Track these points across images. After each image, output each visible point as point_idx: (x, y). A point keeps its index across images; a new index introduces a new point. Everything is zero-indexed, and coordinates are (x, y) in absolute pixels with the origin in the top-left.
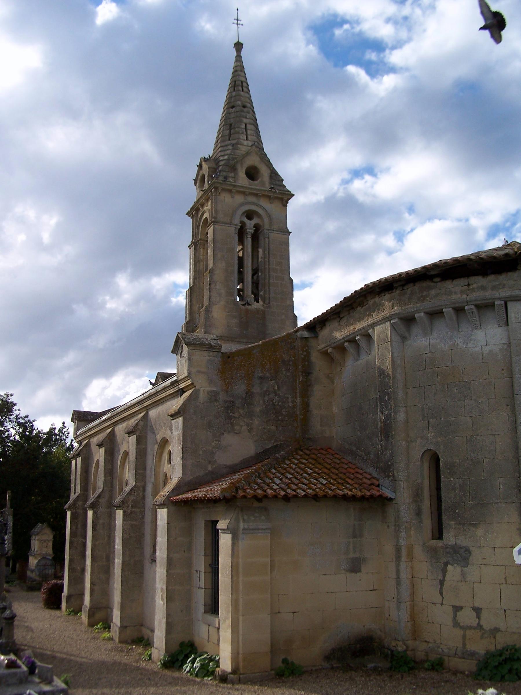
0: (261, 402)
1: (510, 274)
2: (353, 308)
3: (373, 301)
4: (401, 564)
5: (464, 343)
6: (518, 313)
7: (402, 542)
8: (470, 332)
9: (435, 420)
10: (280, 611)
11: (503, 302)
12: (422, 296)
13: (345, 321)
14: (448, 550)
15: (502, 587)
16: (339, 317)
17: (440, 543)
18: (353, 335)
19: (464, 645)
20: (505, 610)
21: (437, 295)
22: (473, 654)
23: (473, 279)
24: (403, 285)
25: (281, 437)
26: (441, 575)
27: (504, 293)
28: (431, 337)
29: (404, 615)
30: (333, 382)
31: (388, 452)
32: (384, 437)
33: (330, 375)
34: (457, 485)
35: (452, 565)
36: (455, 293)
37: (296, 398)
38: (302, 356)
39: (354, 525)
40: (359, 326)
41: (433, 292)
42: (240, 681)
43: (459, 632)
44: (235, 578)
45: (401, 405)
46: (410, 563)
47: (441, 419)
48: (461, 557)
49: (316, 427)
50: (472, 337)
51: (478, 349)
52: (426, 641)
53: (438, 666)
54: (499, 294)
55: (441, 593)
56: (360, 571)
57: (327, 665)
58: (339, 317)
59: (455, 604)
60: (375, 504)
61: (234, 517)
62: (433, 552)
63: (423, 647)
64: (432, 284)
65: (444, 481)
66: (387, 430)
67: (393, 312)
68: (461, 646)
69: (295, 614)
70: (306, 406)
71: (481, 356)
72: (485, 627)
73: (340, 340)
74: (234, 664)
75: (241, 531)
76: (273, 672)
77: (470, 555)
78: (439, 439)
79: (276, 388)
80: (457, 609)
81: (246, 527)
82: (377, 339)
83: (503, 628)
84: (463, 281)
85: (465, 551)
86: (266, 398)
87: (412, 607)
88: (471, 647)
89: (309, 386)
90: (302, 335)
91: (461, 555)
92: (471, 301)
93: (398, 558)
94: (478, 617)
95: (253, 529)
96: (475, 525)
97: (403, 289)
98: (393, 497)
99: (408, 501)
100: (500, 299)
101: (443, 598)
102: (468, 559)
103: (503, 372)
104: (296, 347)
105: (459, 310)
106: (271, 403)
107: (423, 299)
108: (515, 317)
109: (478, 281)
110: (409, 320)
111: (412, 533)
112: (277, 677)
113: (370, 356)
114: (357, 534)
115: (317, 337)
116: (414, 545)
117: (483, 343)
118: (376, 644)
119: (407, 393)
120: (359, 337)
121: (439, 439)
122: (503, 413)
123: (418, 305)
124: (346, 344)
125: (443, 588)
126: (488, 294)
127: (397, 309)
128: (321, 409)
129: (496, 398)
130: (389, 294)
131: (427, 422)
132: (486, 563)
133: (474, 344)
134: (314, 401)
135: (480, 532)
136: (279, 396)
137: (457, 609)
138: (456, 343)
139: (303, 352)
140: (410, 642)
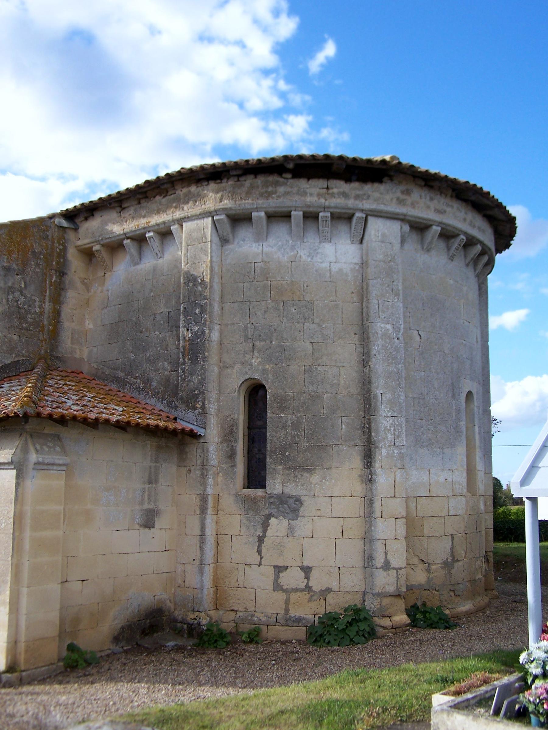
0: (4, 300)
1: (376, 185)
2: (146, 197)
3: (185, 190)
4: (208, 517)
5: (308, 256)
6: (378, 231)
7: (209, 490)
8: (317, 244)
9: (262, 343)
10: (68, 580)
11: (364, 216)
12: (266, 192)
13: (131, 212)
14: (272, 500)
15: (338, 541)
16: (121, 206)
17: (259, 492)
18: (143, 231)
19: (287, 610)
20: (339, 568)
21: (287, 194)
22: (298, 621)
23: (333, 183)
24: (239, 176)
25: (24, 352)
26: (261, 530)
27: (368, 205)
28: (264, 244)
29: (208, 580)
30: (88, 291)
31: (195, 379)
32: (189, 359)
33: (86, 281)
34: (289, 423)
35: (277, 518)
36: (311, 195)
37: (44, 302)
38: (58, 250)
39: (150, 467)
40: (156, 219)
41: (281, 190)
42: (21, 682)
43: (281, 597)
44: (17, 534)
45: (215, 322)
46: (215, 516)
47: (271, 342)
48: (289, 508)
49: (66, 342)
50: (320, 251)
51: (325, 265)
52: (232, 610)
53: (254, 637)
54: (363, 205)
55: (259, 552)
56: (153, 527)
57: (118, 649)
58: (121, 206)
59: (276, 564)
60: (177, 440)
61: (20, 446)
62: (250, 505)
63: (232, 616)
64: (281, 180)
65: (271, 418)
66: (195, 350)
67: (220, 206)
68: (283, 612)
69: (84, 582)
70: (57, 314)
71: (328, 275)
72: (314, 589)
73: (120, 235)
74: (10, 657)
75: (31, 466)
76: (61, 664)
77: (301, 506)
78: (267, 367)
79: (23, 286)
80: (279, 569)
81: (40, 460)
82: (186, 237)
83: (335, 589)
84: (322, 183)
85: (295, 501)
86: (11, 297)
87: (216, 569)
88: (294, 612)
89: (63, 289)
90: (60, 222)
91: (290, 506)
92: (329, 207)
93: (203, 510)
94: (307, 577)
95: (47, 464)
96: (310, 471)
97: (238, 180)
98: (203, 435)
99: (216, 440)
100: (362, 211)
101: (261, 558)
102: (298, 510)
103: (353, 295)
104: (50, 237)
105: (311, 217)
106: (15, 304)
107: (269, 195)
108: (375, 235)
109: (339, 186)
110: (239, 219)
111: (220, 479)
112: (69, 669)
113: (161, 261)
114: (152, 480)
115: (76, 229)
116: (221, 495)
117: (333, 259)
118: (165, 618)
119: (222, 308)
120: (151, 234)
121: (267, 367)
122: (350, 342)
123: (260, 202)
124: (126, 242)
125: (263, 545)
126: (351, 203)
127: (227, 203)
128: (73, 321)
129: (343, 324)
130: (215, 183)
131: (251, 345)
132: (320, 515)
133: (321, 259)
134: (66, 310)
135: (315, 478)
136: (26, 297)
137: (279, 569)
138: (298, 255)
139: (59, 245)
140: (212, 613)
